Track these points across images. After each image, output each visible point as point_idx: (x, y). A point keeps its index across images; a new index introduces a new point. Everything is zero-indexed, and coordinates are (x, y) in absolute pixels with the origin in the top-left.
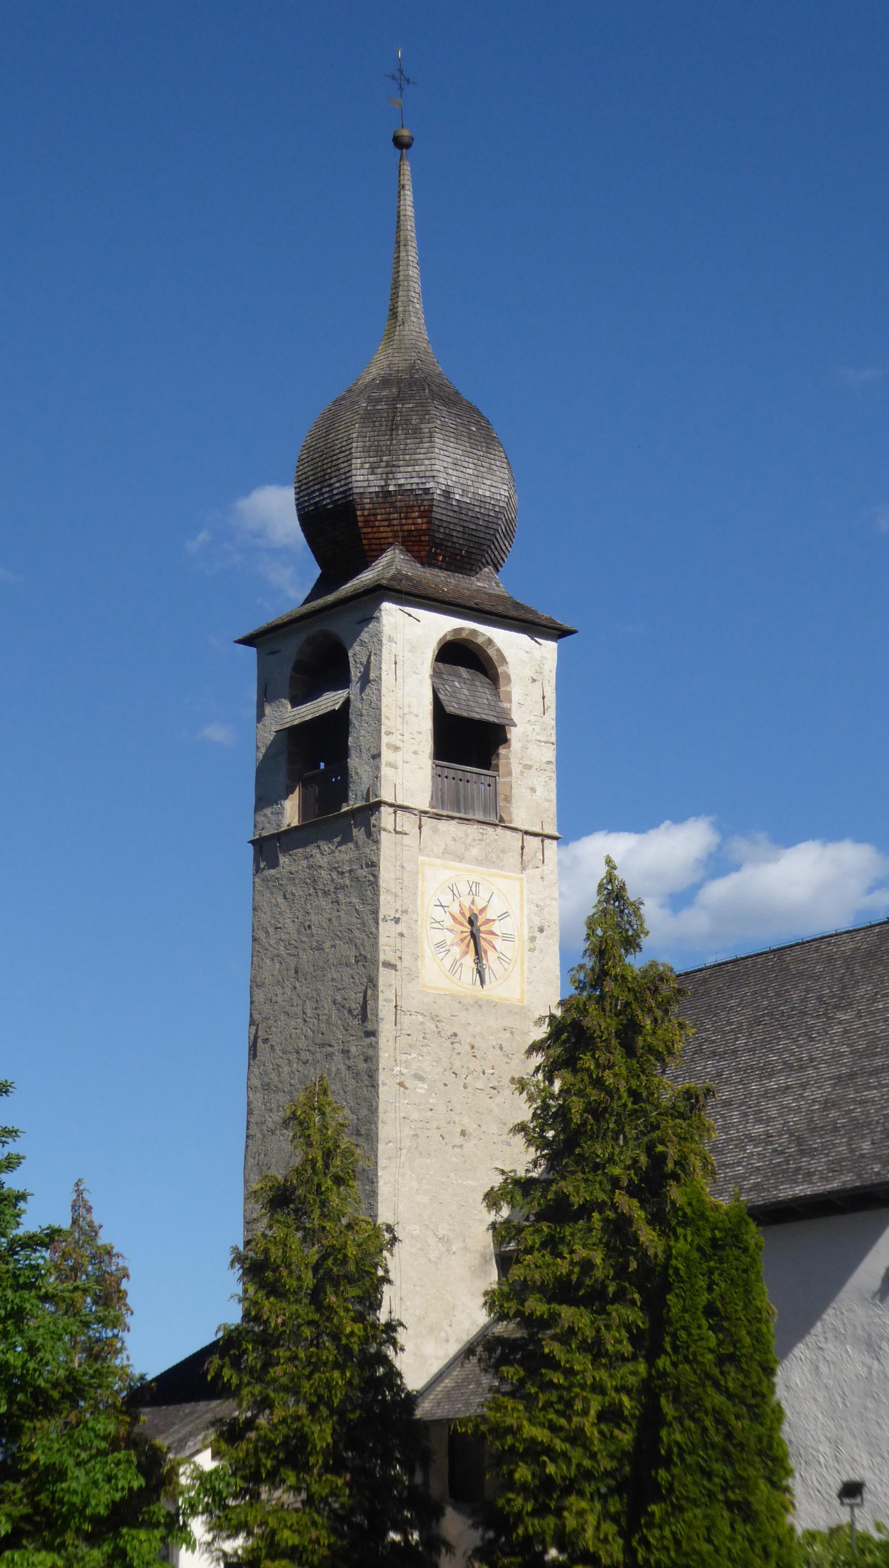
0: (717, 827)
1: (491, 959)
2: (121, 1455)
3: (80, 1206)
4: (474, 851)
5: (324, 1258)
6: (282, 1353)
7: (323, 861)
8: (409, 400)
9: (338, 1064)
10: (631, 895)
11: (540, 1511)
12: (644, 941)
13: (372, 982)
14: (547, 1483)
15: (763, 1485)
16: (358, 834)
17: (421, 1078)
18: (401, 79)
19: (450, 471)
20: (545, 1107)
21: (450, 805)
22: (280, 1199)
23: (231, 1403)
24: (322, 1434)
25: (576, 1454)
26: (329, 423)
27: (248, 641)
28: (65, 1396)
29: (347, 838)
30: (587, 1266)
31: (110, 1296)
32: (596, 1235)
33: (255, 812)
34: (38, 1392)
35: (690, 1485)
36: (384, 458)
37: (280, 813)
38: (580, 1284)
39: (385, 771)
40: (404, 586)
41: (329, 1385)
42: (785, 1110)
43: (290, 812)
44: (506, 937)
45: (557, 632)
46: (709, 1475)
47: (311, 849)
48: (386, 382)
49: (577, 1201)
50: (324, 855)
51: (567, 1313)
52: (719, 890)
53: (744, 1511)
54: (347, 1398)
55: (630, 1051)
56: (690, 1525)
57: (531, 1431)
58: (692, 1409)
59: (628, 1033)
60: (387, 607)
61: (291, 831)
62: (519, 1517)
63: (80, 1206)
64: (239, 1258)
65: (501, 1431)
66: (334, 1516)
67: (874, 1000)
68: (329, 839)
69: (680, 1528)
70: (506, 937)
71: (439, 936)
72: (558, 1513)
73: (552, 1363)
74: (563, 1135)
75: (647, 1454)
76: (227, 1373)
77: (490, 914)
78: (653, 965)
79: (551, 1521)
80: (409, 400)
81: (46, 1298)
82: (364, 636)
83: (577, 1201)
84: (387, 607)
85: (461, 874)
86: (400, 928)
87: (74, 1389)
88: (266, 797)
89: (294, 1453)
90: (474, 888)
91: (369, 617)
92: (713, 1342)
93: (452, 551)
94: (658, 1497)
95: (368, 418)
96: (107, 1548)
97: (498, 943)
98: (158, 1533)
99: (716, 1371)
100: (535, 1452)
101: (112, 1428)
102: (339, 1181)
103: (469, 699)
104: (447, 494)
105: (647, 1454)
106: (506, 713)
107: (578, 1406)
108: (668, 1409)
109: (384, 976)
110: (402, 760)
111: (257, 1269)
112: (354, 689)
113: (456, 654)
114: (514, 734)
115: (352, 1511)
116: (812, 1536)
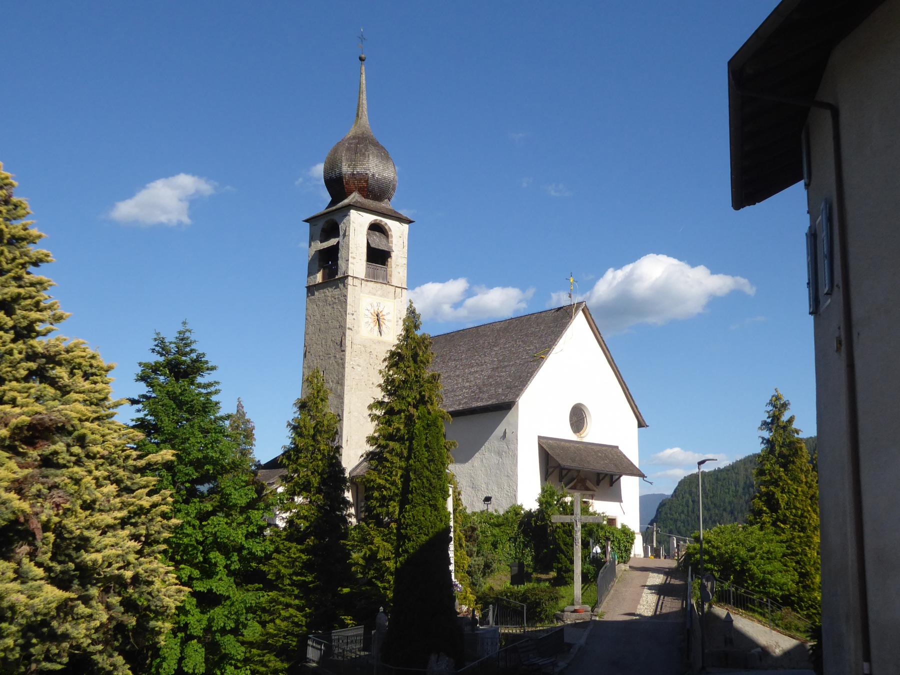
0: (468, 282)
1: (383, 328)
2: (250, 487)
3: (240, 406)
4: (379, 292)
5: (317, 425)
6: (302, 455)
7: (329, 294)
8: (361, 144)
9: (332, 360)
10: (417, 312)
11: (381, 506)
12: (421, 326)
13: (344, 334)
14: (384, 497)
15: (441, 499)
16: (341, 286)
17: (358, 365)
18: (362, 38)
19: (374, 167)
20: (388, 379)
21: (372, 277)
22: (303, 406)
23: (286, 470)
24: (315, 481)
25: (393, 488)
26: (335, 151)
27: (306, 221)
28: (231, 468)
29: (337, 287)
30: (398, 430)
31: (249, 435)
32: (402, 420)
33: (308, 276)
34: (223, 466)
35: (418, 500)
36: (353, 163)
37: (316, 278)
38: (396, 435)
39: (350, 265)
40: (358, 205)
41: (318, 466)
42: (476, 378)
43: (319, 277)
44: (389, 321)
45: (409, 222)
46: (424, 496)
47: (326, 290)
48: (354, 138)
49: (396, 409)
50: (329, 292)
51: (391, 444)
52: (470, 302)
53: (435, 507)
54: (324, 469)
55: (415, 362)
56: (418, 511)
57: (379, 481)
58: (419, 476)
59: (415, 356)
60: (352, 211)
61: (319, 284)
62: (375, 508)
63: (240, 406)
64: (289, 425)
65: (369, 481)
66: (318, 506)
67: (505, 344)
68: (331, 287)
69: (415, 512)
70: (389, 321)
71: (366, 320)
72: (387, 506)
73: (387, 460)
74: (391, 387)
75: (406, 489)
76: (284, 461)
77: (383, 313)
78: (424, 334)
79: (385, 509)
80: (361, 144)
81: (227, 436)
82: (345, 221)
83: (396, 409)
84: (352, 211)
85: (375, 300)
86: (354, 317)
87: (234, 466)
88: (311, 273)
89: (305, 488)
90: (378, 304)
91: (346, 214)
92: (427, 455)
93: (375, 193)
94: (408, 503)
95: (348, 149)
96: (244, 516)
97: (386, 322)
98: (261, 512)
99: (427, 465)
100: (380, 487)
101: (247, 479)
102: (322, 400)
103: (379, 242)
104: (373, 175)
105: (406, 489)
106: (391, 248)
107: (394, 473)
108: (412, 476)
109: (348, 332)
110: (355, 261)
111: (297, 428)
112: (341, 238)
113: (375, 228)
114: (393, 254)
115: (325, 505)
116: (474, 514)
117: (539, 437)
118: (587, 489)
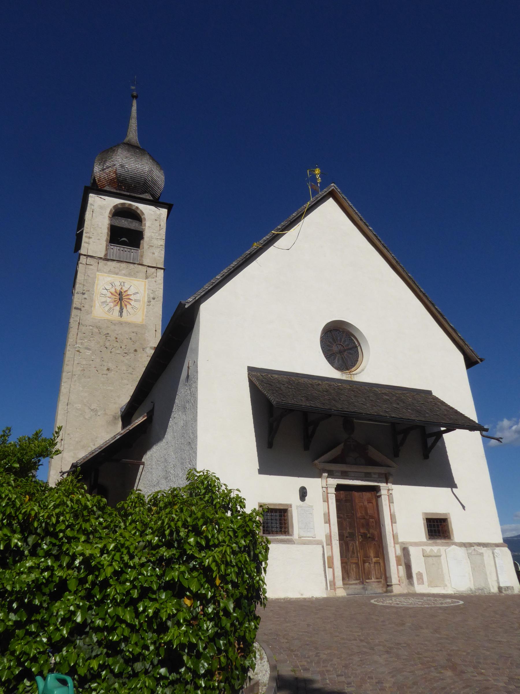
70: (136, 301)
90: (122, 284)
117: (251, 369)
118: (373, 463)
